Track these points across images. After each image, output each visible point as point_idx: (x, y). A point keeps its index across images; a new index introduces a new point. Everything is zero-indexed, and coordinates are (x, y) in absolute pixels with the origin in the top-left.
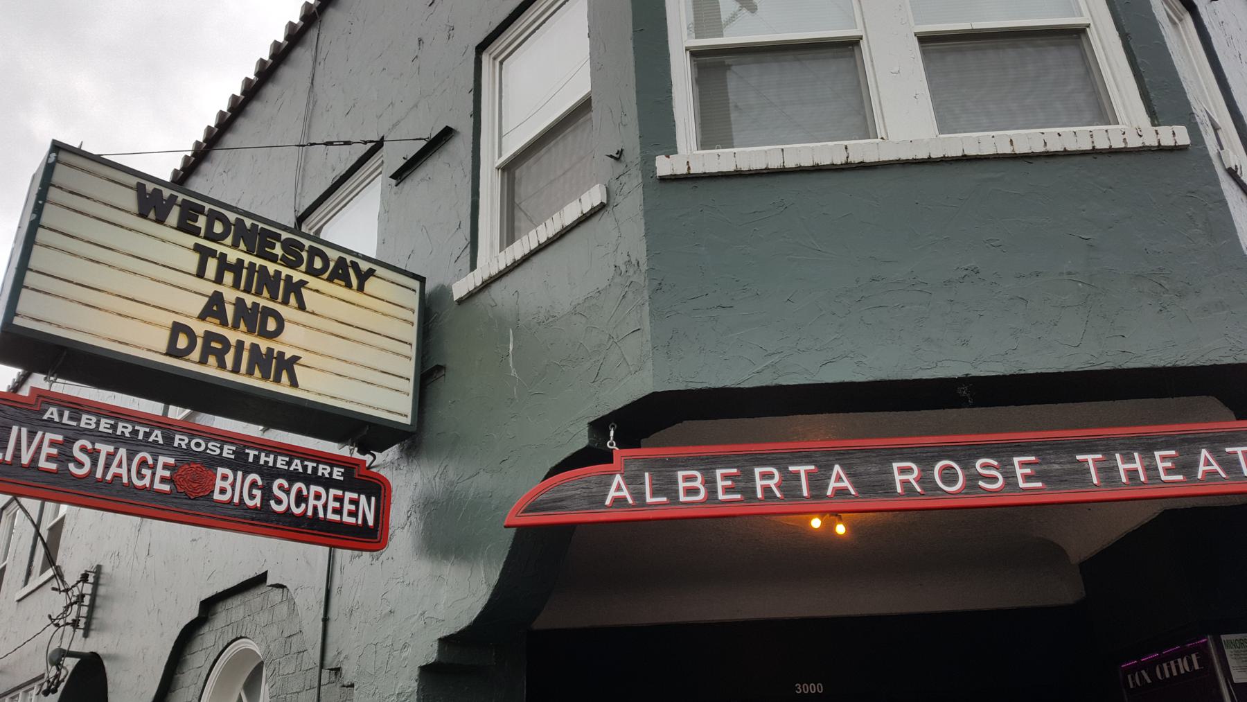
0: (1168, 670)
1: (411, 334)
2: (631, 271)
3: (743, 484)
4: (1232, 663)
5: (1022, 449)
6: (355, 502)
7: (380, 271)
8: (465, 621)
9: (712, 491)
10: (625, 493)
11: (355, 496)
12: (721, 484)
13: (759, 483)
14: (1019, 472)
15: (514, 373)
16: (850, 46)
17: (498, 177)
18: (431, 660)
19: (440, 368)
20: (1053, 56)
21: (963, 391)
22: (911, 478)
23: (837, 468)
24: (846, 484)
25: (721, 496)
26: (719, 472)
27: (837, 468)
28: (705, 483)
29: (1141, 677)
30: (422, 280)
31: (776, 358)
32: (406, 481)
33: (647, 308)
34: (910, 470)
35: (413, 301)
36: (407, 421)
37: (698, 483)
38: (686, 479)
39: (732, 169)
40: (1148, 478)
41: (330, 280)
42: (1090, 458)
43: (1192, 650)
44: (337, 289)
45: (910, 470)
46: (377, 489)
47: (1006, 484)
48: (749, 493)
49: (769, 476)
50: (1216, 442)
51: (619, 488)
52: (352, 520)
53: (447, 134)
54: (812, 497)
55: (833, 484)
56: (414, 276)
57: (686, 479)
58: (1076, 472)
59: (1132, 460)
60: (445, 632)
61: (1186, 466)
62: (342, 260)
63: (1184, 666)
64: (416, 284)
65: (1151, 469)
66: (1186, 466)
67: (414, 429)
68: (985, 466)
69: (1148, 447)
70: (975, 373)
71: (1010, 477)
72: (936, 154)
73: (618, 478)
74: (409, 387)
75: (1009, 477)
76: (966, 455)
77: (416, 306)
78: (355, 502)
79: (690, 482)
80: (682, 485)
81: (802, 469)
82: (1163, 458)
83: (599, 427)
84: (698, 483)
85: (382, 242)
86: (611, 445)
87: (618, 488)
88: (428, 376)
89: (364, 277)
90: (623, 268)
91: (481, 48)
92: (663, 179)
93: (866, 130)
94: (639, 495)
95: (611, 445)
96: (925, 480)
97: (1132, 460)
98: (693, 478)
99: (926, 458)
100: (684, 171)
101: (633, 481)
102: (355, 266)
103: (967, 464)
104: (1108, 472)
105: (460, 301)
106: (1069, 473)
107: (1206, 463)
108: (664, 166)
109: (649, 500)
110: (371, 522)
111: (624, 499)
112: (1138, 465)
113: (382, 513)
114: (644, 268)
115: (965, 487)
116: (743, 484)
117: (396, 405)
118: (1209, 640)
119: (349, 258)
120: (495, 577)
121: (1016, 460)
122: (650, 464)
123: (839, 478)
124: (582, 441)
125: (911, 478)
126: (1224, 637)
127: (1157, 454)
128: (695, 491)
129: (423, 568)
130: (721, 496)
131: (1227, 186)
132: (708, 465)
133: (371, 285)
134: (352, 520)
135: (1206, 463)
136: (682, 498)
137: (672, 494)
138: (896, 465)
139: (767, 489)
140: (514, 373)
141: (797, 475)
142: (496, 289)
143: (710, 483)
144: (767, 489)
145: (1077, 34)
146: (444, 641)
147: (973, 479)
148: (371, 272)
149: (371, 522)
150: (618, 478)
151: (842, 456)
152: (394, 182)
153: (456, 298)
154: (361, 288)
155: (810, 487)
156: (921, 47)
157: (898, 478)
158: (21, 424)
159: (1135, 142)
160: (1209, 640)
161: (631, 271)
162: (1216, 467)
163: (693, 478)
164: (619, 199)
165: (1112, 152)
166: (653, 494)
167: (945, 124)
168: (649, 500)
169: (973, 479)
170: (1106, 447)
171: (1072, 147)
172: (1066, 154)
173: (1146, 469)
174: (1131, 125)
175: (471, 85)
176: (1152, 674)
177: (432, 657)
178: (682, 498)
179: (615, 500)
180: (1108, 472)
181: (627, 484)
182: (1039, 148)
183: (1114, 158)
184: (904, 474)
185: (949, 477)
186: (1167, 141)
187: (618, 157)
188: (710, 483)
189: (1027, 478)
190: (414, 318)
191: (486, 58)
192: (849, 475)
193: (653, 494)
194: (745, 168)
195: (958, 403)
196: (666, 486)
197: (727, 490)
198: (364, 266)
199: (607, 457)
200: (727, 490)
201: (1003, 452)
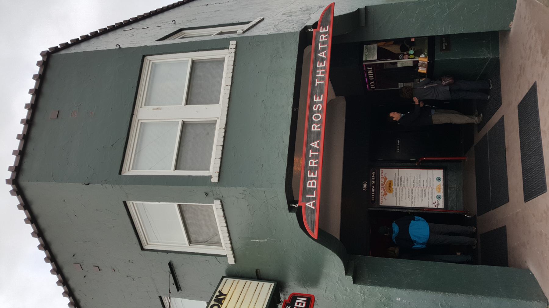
0: (371, 77)
1: (242, 282)
2: (246, 193)
3: (313, 170)
4: (371, 59)
5: (312, 98)
6: (298, 303)
7: (219, 289)
8: (342, 264)
9: (314, 178)
10: (312, 203)
11: (296, 303)
12: (312, 176)
13: (313, 165)
14: (318, 100)
15: (266, 240)
16: (184, 123)
17: (192, 245)
18: (352, 279)
19: (257, 272)
20: (199, 72)
21: (295, 110)
22: (316, 126)
23: (311, 144)
24: (316, 143)
25: (316, 176)
26: (309, 176)
27: (311, 144)
28: (311, 180)
29: (372, 84)
30: (223, 277)
31: (280, 154)
32: (293, 288)
33: (258, 189)
34: (314, 126)
35: (230, 280)
36: (273, 284)
37: (311, 182)
38: (310, 185)
39: (220, 160)
40: (324, 69)
41: (222, 304)
42: (316, 82)
43: (366, 69)
44: (225, 303)
45: (314, 126)
46: (294, 298)
47: (321, 104)
48: (316, 168)
49: (311, 162)
50: (317, 51)
51: (310, 204)
52: (304, 304)
53: (170, 265)
54: (319, 152)
55: (316, 146)
56: (222, 279)
57: (310, 185)
58: (320, 87)
59: (319, 73)
60: (344, 272)
61: (322, 60)
62: (215, 300)
63: (370, 72)
64: (225, 279)
65: (322, 68)
66: (322, 60)
67: (276, 283)
68: (315, 108)
69: (316, 68)
70: (292, 105)
71: (319, 103)
72: (227, 105)
73: (307, 204)
74: (261, 283)
75: (319, 103)
76: (312, 112)
77: (232, 280)
78: (298, 303)
79: (310, 184)
80: (311, 186)
81: (311, 153)
82: (319, 65)
83: (291, 209)
84: (311, 182)
85: (201, 299)
86: (296, 206)
87: (310, 205)
88: (258, 277)
89: (221, 294)
90: (244, 196)
91: (142, 249)
92: (218, 180)
93: (213, 124)
94: (313, 199)
95: (296, 206)
96: (317, 123)
97: (319, 73)
98: (310, 183)
99: (311, 122)
100: (218, 174)
101: (309, 200)
102: (217, 296)
103: (315, 112)
104: (321, 79)
105: (235, 262)
106: (320, 88)
107: (322, 55)
108: (215, 179)
109: (314, 196)
110: (305, 299)
111: (313, 203)
112: (320, 71)
113: (302, 296)
114: (246, 188)
115: (320, 114)
116: (313, 170)
117: (267, 288)
118: (364, 64)
119: (214, 298)
120: (330, 251)
121: (315, 100)
122: (304, 195)
123: (314, 144)
124: (294, 215)
125: (316, 126)
126: (364, 60)
127: (318, 66)
128: (313, 183)
129: (323, 283)
130: (316, 176)
131: (246, 35)
132: (306, 179)
133: (224, 292)
134: (304, 304)
135: (322, 55)
136: (315, 187)
137: (314, 189)
138: (312, 130)
139: (315, 164)
140: (266, 240)
141: (312, 155)
142: (235, 247)
143: (312, 179)
144: (315, 164)
145: (194, 62)
146: (347, 274)
147: (318, 111)
148: (220, 292)
149: (305, 299)
150: (307, 204)
151: (308, 143)
152: (180, 291)
153: (234, 263)
154: (225, 295)
155: (316, 152)
156: (190, 104)
157: (316, 130)
158: (373, 69)
159: (233, 55)
160: (364, 64)
161: (246, 193)
162: (323, 53)
163: (310, 183)
164: (221, 195)
165: (234, 61)
166: (313, 195)
167: (216, 101)
168: (314, 196)
169: (318, 111)
170: (314, 78)
171: (232, 71)
172: (233, 72)
173: (321, 69)
174: (227, 56)
175: (156, 253)
176: (372, 81)
177: (350, 278)
178: (315, 187)
179: (313, 206)
180: (321, 79)
181: (309, 202)
182: (230, 79)
183: (236, 61)
184: (315, 128)
185: (317, 117)
186: (234, 46)
187: (207, 194)
188: (312, 179)
189: (320, 98)
190: (237, 280)
191: (145, 248)
192: (314, 142)
193: (313, 195)
194: (220, 156)
195: (297, 111)
196: (311, 191)
197: (314, 174)
198: (217, 294)
199: (300, 208)
200: (314, 174)
201: (312, 103)
